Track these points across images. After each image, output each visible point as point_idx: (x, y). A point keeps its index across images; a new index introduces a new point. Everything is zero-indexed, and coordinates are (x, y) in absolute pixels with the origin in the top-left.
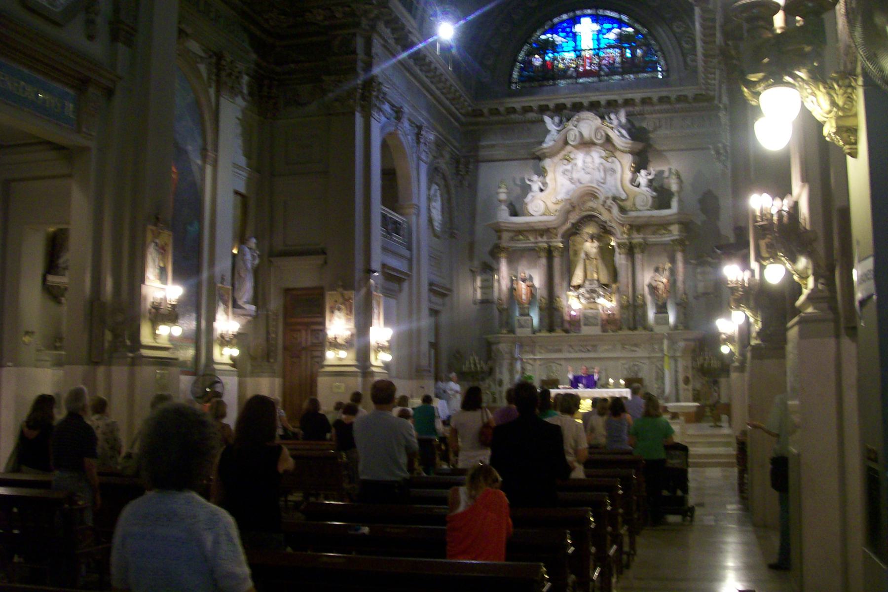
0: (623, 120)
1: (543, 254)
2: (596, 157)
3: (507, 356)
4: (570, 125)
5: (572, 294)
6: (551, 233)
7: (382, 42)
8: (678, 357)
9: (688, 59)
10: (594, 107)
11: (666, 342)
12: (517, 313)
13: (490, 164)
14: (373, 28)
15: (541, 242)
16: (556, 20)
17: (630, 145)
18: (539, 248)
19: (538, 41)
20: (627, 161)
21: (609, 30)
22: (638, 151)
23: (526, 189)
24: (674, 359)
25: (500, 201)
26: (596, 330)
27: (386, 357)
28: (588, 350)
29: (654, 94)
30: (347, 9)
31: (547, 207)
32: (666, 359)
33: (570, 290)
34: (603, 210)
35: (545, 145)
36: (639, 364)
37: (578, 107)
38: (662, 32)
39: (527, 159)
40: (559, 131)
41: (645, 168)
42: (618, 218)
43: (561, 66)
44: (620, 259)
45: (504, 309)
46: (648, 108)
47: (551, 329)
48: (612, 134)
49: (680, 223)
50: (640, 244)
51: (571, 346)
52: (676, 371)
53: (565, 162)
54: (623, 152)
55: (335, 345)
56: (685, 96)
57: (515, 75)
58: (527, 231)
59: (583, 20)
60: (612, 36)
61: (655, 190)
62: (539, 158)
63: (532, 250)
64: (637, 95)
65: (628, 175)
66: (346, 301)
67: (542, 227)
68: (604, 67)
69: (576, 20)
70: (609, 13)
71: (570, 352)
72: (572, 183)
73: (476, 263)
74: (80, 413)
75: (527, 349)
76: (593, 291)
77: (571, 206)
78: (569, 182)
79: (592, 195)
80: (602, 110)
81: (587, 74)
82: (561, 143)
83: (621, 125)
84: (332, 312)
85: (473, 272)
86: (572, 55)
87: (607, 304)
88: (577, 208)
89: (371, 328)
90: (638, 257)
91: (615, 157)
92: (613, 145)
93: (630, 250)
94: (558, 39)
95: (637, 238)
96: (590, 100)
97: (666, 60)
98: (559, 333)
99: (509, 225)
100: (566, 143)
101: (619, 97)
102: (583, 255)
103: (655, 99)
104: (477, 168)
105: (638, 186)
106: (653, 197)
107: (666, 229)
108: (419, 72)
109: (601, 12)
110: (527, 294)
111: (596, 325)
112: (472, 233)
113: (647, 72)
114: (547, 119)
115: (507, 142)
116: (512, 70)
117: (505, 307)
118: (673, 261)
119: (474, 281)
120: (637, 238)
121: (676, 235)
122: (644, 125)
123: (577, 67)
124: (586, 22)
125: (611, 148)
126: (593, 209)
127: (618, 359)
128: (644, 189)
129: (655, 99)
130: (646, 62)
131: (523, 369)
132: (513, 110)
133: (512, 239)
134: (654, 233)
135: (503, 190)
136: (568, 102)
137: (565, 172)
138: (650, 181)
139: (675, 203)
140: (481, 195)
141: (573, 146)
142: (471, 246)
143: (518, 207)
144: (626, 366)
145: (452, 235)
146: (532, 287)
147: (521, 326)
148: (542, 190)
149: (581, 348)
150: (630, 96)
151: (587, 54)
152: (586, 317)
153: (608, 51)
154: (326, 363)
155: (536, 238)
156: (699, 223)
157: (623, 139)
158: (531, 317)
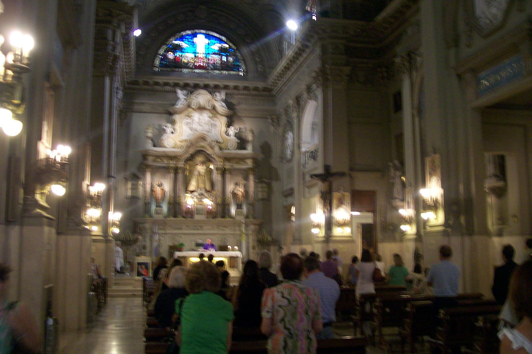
2: (205, 117)
3: (149, 231)
4: (193, 96)
10: (206, 87)
14: (119, 27)
17: (225, 112)
20: (223, 120)
23: (162, 131)
24: (247, 235)
25: (148, 137)
28: (198, 229)
29: (241, 84)
33: (187, 193)
34: (208, 148)
36: (227, 238)
37: (196, 87)
39: (161, 113)
44: (217, 177)
46: (236, 92)
47: (175, 216)
51: (188, 226)
58: (162, 156)
62: (171, 114)
63: (164, 168)
64: (232, 84)
65: (224, 129)
67: (173, 155)
69: (195, 35)
71: (187, 229)
72: (191, 130)
76: (202, 194)
77: (191, 144)
79: (203, 138)
81: (200, 67)
86: (193, 56)
87: (208, 203)
90: (228, 176)
93: (223, 172)
94: (184, 44)
95: (228, 166)
97: (246, 65)
99: (154, 152)
100: (189, 106)
101: (221, 83)
111: (202, 214)
113: (234, 71)
118: (246, 178)
120: (228, 166)
126: (203, 147)
130: (234, 65)
132: (157, 84)
134: (237, 163)
137: (187, 124)
143: (156, 142)
151: (200, 56)
152: (197, 209)
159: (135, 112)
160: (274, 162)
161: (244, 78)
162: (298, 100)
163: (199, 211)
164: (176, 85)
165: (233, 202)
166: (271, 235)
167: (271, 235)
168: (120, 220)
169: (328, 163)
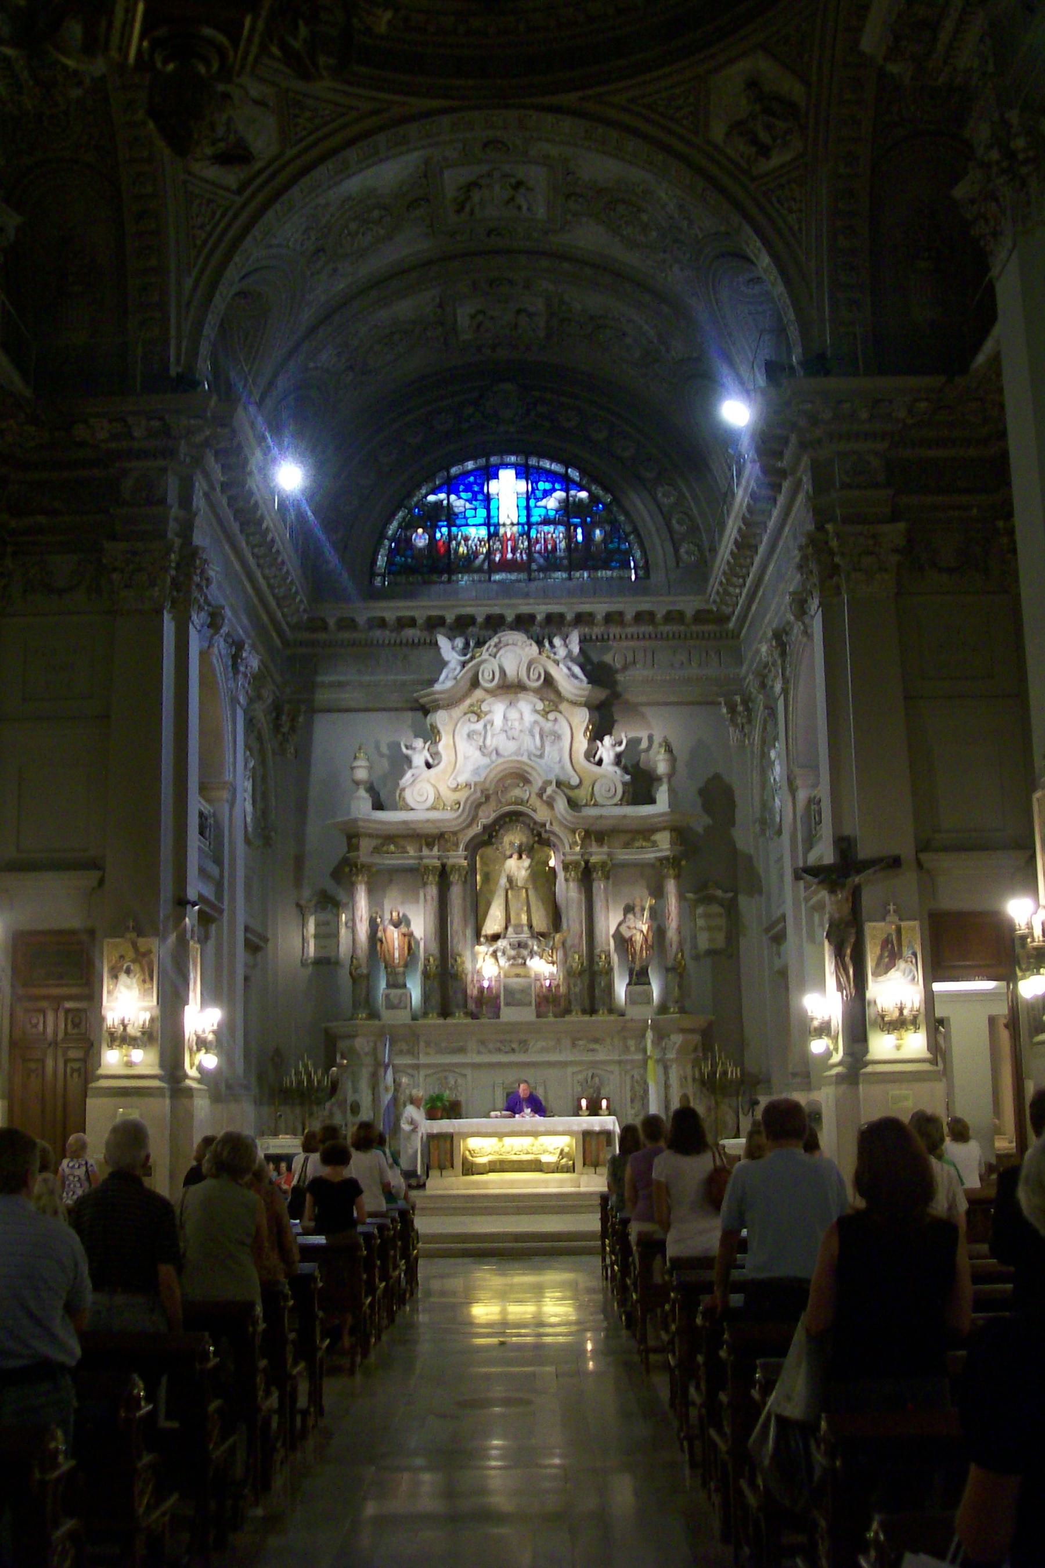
0: (576, 650)
1: (432, 878)
4: (484, 653)
5: (483, 949)
6: (446, 841)
7: (206, 488)
8: (669, 1060)
9: (682, 550)
10: (523, 623)
11: (649, 1034)
12: (383, 984)
13: (346, 716)
14: (198, 461)
15: (428, 857)
16: (454, 470)
18: (426, 867)
19: (422, 503)
20: (581, 718)
21: (547, 493)
22: (598, 702)
23: (402, 763)
25: (357, 783)
26: (527, 1014)
27: (210, 1061)
28: (513, 1050)
29: (630, 606)
30: (156, 424)
31: (438, 797)
32: (650, 1063)
33: (479, 943)
34: (535, 801)
35: (437, 687)
37: (495, 624)
38: (638, 504)
40: (464, 664)
41: (610, 734)
42: (566, 819)
43: (462, 549)
44: (567, 890)
45: (361, 976)
46: (615, 630)
47: (445, 1013)
48: (553, 671)
49: (674, 829)
50: (604, 864)
51: (482, 1042)
52: (667, 1086)
53: (474, 718)
54: (574, 703)
55: (122, 1039)
56: (681, 614)
57: (381, 561)
58: (398, 836)
59: (502, 473)
60: (552, 503)
61: (626, 770)
62: (425, 711)
63: (412, 870)
65: (582, 744)
66: (142, 957)
68: (536, 555)
69: (492, 473)
70: (546, 464)
71: (479, 1052)
72: (484, 755)
73: (307, 893)
74: (139, 1172)
75: (404, 1047)
76: (520, 945)
78: (478, 753)
79: (520, 776)
80: (537, 629)
81: (506, 566)
82: (465, 684)
83: (569, 655)
84: (115, 977)
85: (302, 911)
86: (483, 532)
88: (493, 798)
89: (187, 1008)
90: (599, 886)
91: (561, 712)
92: (558, 693)
93: (586, 875)
94: (458, 503)
95: (598, 855)
96: (519, 612)
98: (460, 1019)
102: (503, 881)
103: (629, 617)
104: (309, 726)
105: (600, 763)
106: (625, 784)
107: (647, 839)
108: (244, 543)
109: (533, 461)
110: (401, 949)
112: (300, 838)
113: (612, 569)
114: (443, 642)
115: (366, 678)
116: (376, 553)
117: (365, 971)
118: (658, 892)
119: (304, 925)
120: (598, 855)
121: (666, 850)
122: (608, 658)
123: (489, 553)
124: (507, 475)
125: (552, 696)
126: (520, 802)
127: (564, 1064)
128: (608, 766)
129: (629, 617)
131: (397, 1085)
132: (382, 623)
133: (377, 850)
134: (627, 845)
135: (361, 762)
136: (480, 613)
138: (618, 757)
139: (662, 795)
140: (318, 772)
141: (486, 690)
142: (299, 861)
143: (383, 796)
144: (580, 1077)
145: (267, 842)
146: (410, 935)
147: (390, 1006)
148: (429, 766)
149: (498, 1045)
150: (586, 608)
152: (509, 991)
153: (546, 528)
154: (101, 1071)
155: (421, 850)
156: (700, 830)
157: (576, 681)
158: (409, 989)
159: (321, 711)
160: (743, 837)
161: (641, 587)
162: (780, 638)
163: (514, 997)
164: (435, 624)
165: (619, 966)
166: (740, 1063)
167: (740, 1063)
168: (215, 1027)
169: (847, 831)
